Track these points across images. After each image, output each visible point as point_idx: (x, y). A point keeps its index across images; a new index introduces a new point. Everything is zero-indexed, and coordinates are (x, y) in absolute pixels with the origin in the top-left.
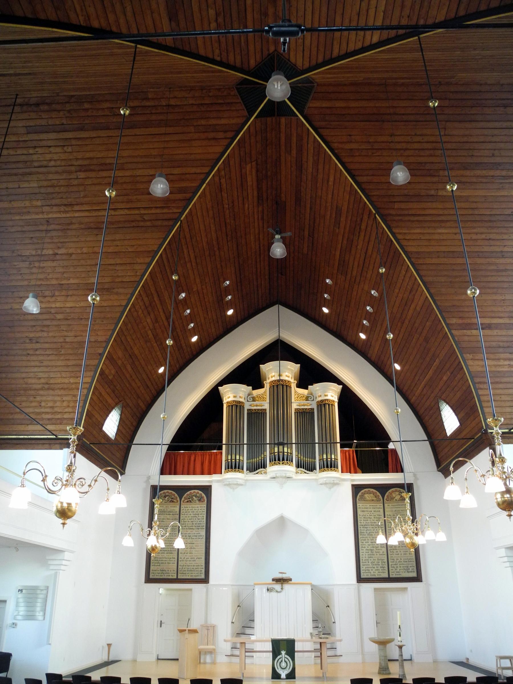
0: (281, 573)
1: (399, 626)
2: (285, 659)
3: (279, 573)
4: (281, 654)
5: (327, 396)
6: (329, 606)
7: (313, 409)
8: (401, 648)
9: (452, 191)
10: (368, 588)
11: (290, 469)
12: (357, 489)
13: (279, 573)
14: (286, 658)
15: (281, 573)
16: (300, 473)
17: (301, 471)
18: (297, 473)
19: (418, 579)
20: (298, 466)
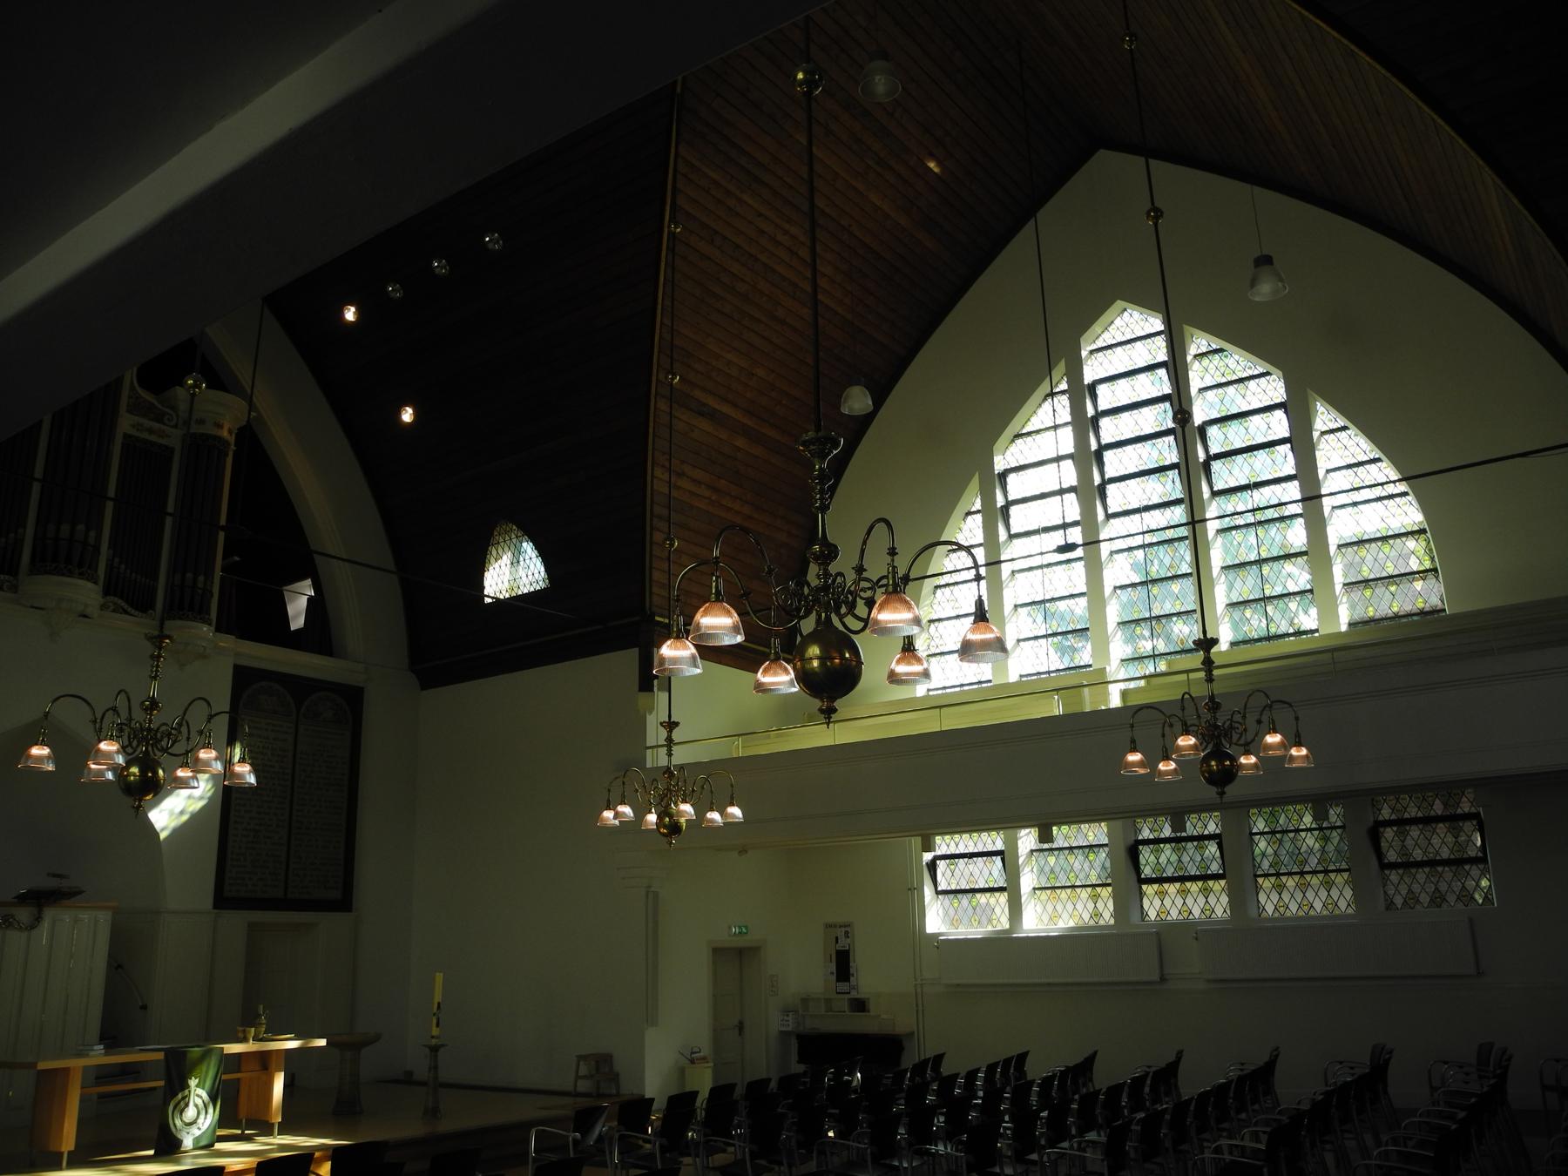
0: (55, 876)
1: (439, 1004)
2: (196, 1098)
3: (48, 874)
4: (188, 1087)
5: (133, 426)
6: (119, 966)
7: (172, 450)
8: (437, 1050)
9: (1131, 49)
10: (236, 921)
11: (87, 593)
12: (244, 678)
13: (48, 874)
14: (198, 1096)
15: (55, 876)
16: (112, 608)
17: (115, 604)
18: (103, 607)
19: (344, 903)
20: (107, 592)
